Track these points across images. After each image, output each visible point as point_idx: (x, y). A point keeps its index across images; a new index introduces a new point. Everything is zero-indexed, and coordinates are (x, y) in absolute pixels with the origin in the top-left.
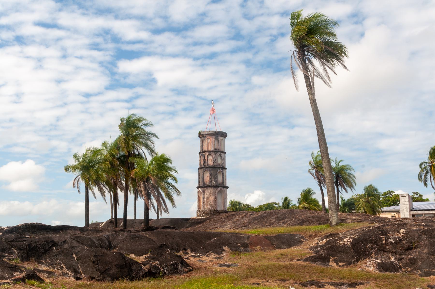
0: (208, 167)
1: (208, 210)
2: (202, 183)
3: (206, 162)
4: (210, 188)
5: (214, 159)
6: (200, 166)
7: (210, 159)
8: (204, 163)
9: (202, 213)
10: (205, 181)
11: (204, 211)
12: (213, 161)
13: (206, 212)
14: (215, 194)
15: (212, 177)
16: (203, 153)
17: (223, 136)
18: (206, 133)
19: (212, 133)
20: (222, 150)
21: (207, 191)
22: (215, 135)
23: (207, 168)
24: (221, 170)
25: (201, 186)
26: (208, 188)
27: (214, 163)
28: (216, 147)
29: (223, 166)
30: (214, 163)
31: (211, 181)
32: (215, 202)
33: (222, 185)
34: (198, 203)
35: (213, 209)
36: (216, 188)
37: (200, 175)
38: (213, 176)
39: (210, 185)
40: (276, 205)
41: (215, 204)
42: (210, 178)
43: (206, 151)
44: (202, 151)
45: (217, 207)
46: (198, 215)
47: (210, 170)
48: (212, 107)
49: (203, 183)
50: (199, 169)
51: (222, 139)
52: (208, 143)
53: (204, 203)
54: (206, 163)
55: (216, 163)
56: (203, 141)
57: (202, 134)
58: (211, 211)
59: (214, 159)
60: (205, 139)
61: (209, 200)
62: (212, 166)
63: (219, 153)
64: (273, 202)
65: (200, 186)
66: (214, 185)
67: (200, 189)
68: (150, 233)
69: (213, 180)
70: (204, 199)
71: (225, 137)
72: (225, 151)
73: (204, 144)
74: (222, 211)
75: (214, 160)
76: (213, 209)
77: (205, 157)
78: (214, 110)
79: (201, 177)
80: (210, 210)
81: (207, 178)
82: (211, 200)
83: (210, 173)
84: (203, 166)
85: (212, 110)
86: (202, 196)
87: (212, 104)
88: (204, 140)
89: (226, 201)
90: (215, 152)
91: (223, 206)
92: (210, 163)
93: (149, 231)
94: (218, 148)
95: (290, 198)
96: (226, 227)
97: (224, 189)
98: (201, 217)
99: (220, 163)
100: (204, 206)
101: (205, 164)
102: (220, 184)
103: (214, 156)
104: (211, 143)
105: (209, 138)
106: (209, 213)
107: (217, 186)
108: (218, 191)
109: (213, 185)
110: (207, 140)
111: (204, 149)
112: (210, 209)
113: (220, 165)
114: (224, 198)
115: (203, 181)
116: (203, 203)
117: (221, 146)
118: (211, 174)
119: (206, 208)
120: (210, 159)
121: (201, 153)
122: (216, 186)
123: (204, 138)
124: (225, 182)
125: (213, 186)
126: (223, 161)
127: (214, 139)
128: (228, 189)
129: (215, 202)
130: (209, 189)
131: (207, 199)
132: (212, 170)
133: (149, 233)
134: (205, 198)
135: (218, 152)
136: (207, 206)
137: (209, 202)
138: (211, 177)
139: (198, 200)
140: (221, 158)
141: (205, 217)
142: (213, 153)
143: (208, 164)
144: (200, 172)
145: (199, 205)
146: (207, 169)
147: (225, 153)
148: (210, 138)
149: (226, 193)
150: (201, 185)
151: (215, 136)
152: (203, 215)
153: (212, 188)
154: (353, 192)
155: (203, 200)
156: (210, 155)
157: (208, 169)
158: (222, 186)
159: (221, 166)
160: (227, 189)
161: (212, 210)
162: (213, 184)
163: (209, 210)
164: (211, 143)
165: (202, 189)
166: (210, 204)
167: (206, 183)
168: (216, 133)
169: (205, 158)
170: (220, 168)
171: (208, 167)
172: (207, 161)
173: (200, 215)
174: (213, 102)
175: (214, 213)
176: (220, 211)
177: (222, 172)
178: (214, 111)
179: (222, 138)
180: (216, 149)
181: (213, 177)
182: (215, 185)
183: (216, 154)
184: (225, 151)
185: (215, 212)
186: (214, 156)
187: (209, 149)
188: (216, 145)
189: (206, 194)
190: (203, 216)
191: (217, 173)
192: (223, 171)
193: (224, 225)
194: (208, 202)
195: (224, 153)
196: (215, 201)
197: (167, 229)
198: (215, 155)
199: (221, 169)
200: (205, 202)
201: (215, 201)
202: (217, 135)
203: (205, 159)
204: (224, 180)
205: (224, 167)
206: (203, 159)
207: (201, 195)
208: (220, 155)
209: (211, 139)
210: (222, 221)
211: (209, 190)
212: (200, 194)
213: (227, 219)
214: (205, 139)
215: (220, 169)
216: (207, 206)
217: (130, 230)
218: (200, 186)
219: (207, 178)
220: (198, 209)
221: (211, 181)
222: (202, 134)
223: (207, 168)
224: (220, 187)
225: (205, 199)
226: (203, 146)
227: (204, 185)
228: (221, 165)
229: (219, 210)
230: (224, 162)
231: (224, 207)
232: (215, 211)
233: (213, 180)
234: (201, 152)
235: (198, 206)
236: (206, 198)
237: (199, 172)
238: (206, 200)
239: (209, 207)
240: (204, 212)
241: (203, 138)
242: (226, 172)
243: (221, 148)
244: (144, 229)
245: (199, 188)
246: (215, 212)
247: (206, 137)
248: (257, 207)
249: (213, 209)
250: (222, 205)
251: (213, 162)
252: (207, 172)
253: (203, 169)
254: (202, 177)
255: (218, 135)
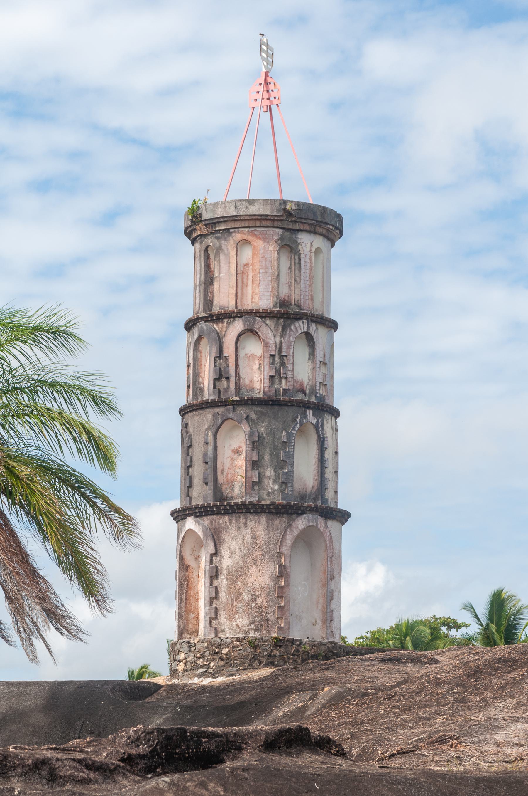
0: (241, 403)
1: (238, 640)
2: (206, 488)
3: (228, 372)
4: (249, 516)
5: (273, 356)
6: (195, 396)
7: (253, 356)
8: (215, 380)
9: (202, 656)
10: (221, 479)
11: (219, 646)
12: (270, 368)
13: (225, 651)
14: (280, 553)
15: (261, 457)
16: (212, 321)
17: (325, 232)
18: (232, 212)
19: (266, 211)
20: (317, 309)
21: (233, 533)
22: (279, 224)
23: (235, 404)
24: (314, 421)
25: (203, 507)
26: (242, 520)
27: (272, 377)
28: (284, 292)
29: (322, 398)
30: (272, 377)
31: (255, 479)
32: (280, 597)
33: (319, 503)
34: (180, 603)
35: (266, 636)
36: (285, 518)
37: (195, 443)
38: (268, 451)
39: (251, 503)
40: (453, 630)
41: (281, 608)
42: (255, 465)
43: (232, 312)
44: (205, 311)
45: (288, 624)
46: (181, 667)
47: (253, 416)
48: (264, 70)
49: (208, 491)
50: (184, 411)
51: (316, 245)
52: (241, 268)
53: (216, 603)
54: (228, 378)
55: (284, 381)
56: (212, 256)
57: (206, 216)
58: (255, 647)
59: (273, 356)
60: (224, 243)
61: (245, 584)
62: (261, 395)
63: (301, 326)
64: (437, 616)
65: (197, 507)
66: (273, 504)
67: (190, 523)
68: (211, 785)
69: (268, 473)
70: (217, 577)
71: (332, 237)
72: (329, 311)
73: (216, 274)
74: (313, 645)
75: (272, 363)
76: (269, 633)
77: (225, 346)
78: (271, 87)
79: (201, 456)
80: (250, 642)
81: (233, 459)
82: (257, 585)
83: (251, 435)
84: (208, 395)
85: (261, 89)
86: (204, 560)
87: (264, 55)
88: (219, 250)
89: (336, 594)
90: (278, 318)
91: (319, 622)
92: (251, 381)
93: (177, 771)
94: (296, 295)
95: (170, 638)
96: (500, 737)
97: (330, 523)
98: (200, 676)
99: (306, 383)
100: (216, 617)
101: (224, 383)
102: (303, 497)
103: (272, 342)
104: (257, 267)
105: (246, 242)
106: (243, 658)
107: (289, 504)
108: (296, 533)
109: (268, 502)
110: (233, 253)
111: (216, 302)
112: (248, 633)
113: (304, 392)
114: (325, 573)
115: (210, 480)
116: (213, 598)
117: (311, 284)
118: (257, 439)
119: (226, 628)
120: (250, 357)
121: (202, 324)
122: (283, 506)
123: (218, 238)
124: (330, 485)
125: (268, 506)
126: (323, 370)
127: (272, 248)
128: (345, 528)
129: (280, 597)
130: (245, 524)
131: (232, 580)
132: (261, 416)
133: (203, 785)
134: (225, 572)
135: (298, 317)
136: (231, 618)
137: (246, 597)
138: (255, 458)
139: (181, 585)
140: (312, 354)
141: (221, 680)
142: (268, 321)
143: (238, 388)
144: (191, 429)
145: (188, 611)
146: (234, 410)
147: (333, 325)
148: (250, 238)
149: (336, 545)
150: (198, 501)
151: (280, 231)
152: (208, 666)
153: (263, 518)
154: (52, 655)
155: (211, 584)
156: (251, 331)
157: (242, 411)
158: (316, 510)
159: (313, 399)
160: (343, 524)
161: (262, 639)
162: (269, 494)
163: (244, 638)
164: (257, 267)
165: (206, 521)
166: (248, 605)
167: (226, 491)
168: (289, 214)
169: (221, 350)
170: (305, 405)
171: (241, 403)
172: (237, 366)
173: (193, 669)
174: (267, 45)
175: (275, 656)
176: (308, 647)
177: (318, 428)
178: (273, 94)
179: (319, 242)
180: (283, 303)
181: (267, 458)
182: (279, 499)
183: (284, 329)
184: (333, 317)
185: (276, 652)
186: (272, 342)
187: (249, 304)
188: (284, 278)
189: (225, 552)
190: (213, 675)
191: (289, 436)
192: (322, 426)
193: (480, 725)
194: (238, 595)
195: (328, 326)
196: (280, 588)
197: (298, 755)
198: (281, 337)
199: (313, 415)
200: (223, 595)
201: (280, 588)
202: (291, 226)
203: (225, 354)
204: (329, 473)
205: (327, 401)
206: (214, 354)
207: (197, 558)
208: (309, 337)
209: (259, 243)
210: (451, 699)
211: (244, 531)
212: (193, 551)
213: (476, 690)
214: (224, 247)
215: (306, 416)
216: (231, 618)
217: (44, 762)
218: (191, 508)
219: (233, 459)
220: (181, 635)
221: (255, 479)
222: (206, 216)
223: (235, 404)
224: (303, 513)
225: (223, 581)
226: (212, 283)
227: (215, 499)
228: (313, 392)
229: (301, 642)
230: (325, 375)
231: (324, 622)
232: (275, 645)
233: (269, 472)
234: (202, 315)
235: (180, 616)
236: (229, 573)
237: (185, 426)
238: (229, 587)
239: (243, 621)
240: (215, 653)
241: (210, 241)
242: (337, 430)
243: (312, 299)
244: (143, 749)
245: (190, 515)
246: (276, 652)
247: (230, 234)
248: (362, 638)
249: (269, 633)
250: (318, 615)
251: (269, 371)
252: (234, 427)
253: (209, 414)
254: (205, 455)
255: (297, 227)
